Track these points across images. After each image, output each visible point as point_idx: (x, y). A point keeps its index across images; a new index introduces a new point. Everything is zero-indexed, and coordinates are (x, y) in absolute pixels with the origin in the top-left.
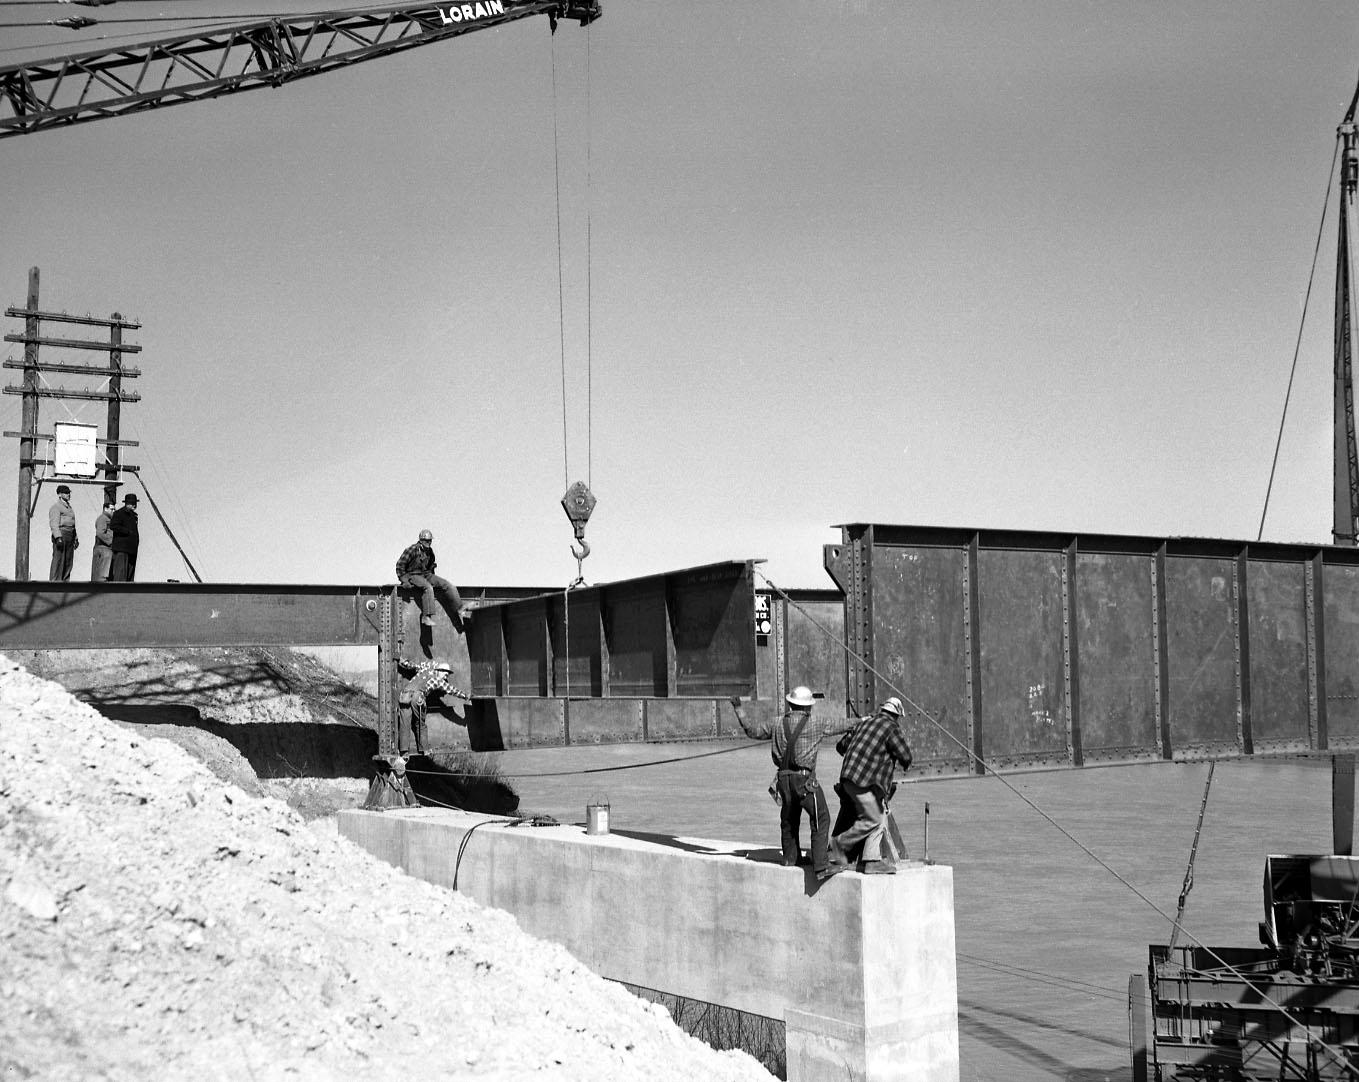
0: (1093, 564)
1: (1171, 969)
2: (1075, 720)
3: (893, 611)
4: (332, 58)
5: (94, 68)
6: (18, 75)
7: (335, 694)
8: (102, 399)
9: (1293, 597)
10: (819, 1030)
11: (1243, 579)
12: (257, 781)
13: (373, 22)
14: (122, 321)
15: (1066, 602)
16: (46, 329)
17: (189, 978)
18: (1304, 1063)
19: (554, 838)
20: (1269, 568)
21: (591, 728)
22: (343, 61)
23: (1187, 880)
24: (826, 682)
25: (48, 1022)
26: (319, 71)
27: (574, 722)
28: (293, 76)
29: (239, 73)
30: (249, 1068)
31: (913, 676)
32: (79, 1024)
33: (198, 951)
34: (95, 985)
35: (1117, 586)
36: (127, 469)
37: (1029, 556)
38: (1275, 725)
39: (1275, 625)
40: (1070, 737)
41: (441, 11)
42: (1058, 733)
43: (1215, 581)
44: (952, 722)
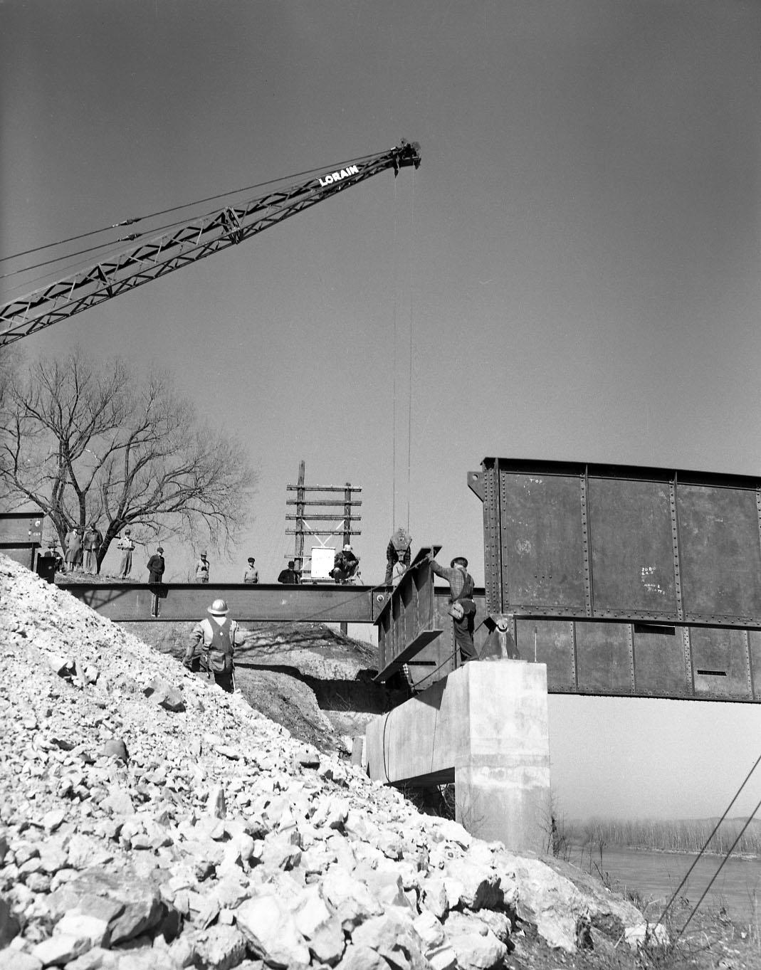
7: (324, 638)
12: (317, 706)
14: (350, 487)
16: (308, 496)
24: (728, 664)
31: (539, 553)
41: (320, 180)
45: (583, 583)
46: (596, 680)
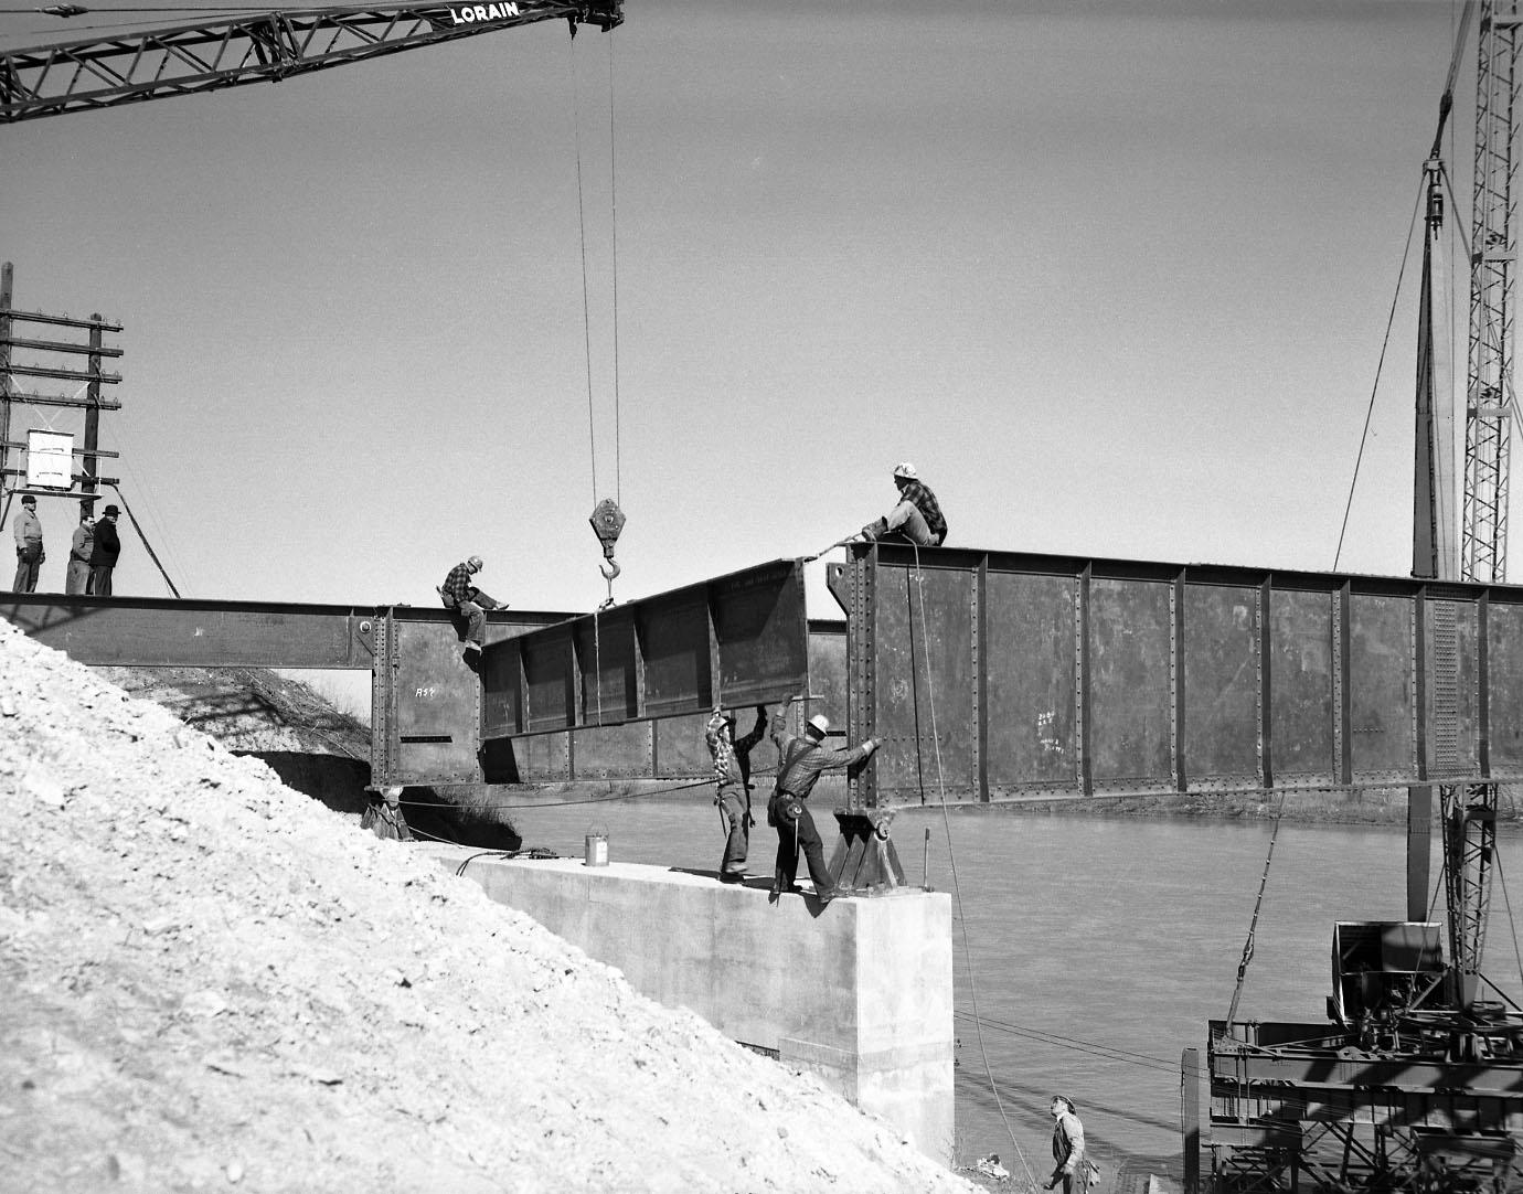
0: (1109, 590)
1: (1225, 1046)
2: (1086, 749)
3: (897, 634)
4: (336, 54)
5: (83, 58)
6: (4, 63)
8: (79, 405)
9: (1319, 627)
10: (813, 1058)
11: (1266, 608)
13: (380, 19)
14: (103, 323)
15: (1079, 628)
17: (176, 858)
18: (1372, 1149)
19: (554, 869)
20: (1293, 597)
21: (596, 763)
22: (347, 58)
23: (1247, 948)
25: (61, 873)
26: (322, 66)
27: (580, 756)
28: (293, 71)
29: (238, 67)
30: (225, 919)
32: (86, 877)
33: (183, 842)
34: (100, 852)
35: (1133, 614)
36: (106, 482)
37: (1042, 580)
38: (1297, 758)
39: (1299, 655)
40: (1080, 766)
41: (453, 12)
42: (1068, 763)
43: (1240, 609)
44: (957, 748)
45: (970, 746)
46: (680, 754)
